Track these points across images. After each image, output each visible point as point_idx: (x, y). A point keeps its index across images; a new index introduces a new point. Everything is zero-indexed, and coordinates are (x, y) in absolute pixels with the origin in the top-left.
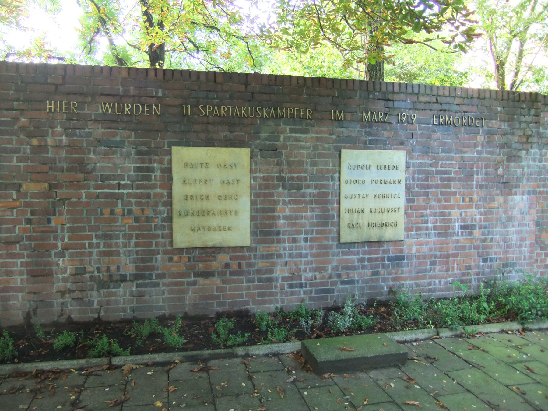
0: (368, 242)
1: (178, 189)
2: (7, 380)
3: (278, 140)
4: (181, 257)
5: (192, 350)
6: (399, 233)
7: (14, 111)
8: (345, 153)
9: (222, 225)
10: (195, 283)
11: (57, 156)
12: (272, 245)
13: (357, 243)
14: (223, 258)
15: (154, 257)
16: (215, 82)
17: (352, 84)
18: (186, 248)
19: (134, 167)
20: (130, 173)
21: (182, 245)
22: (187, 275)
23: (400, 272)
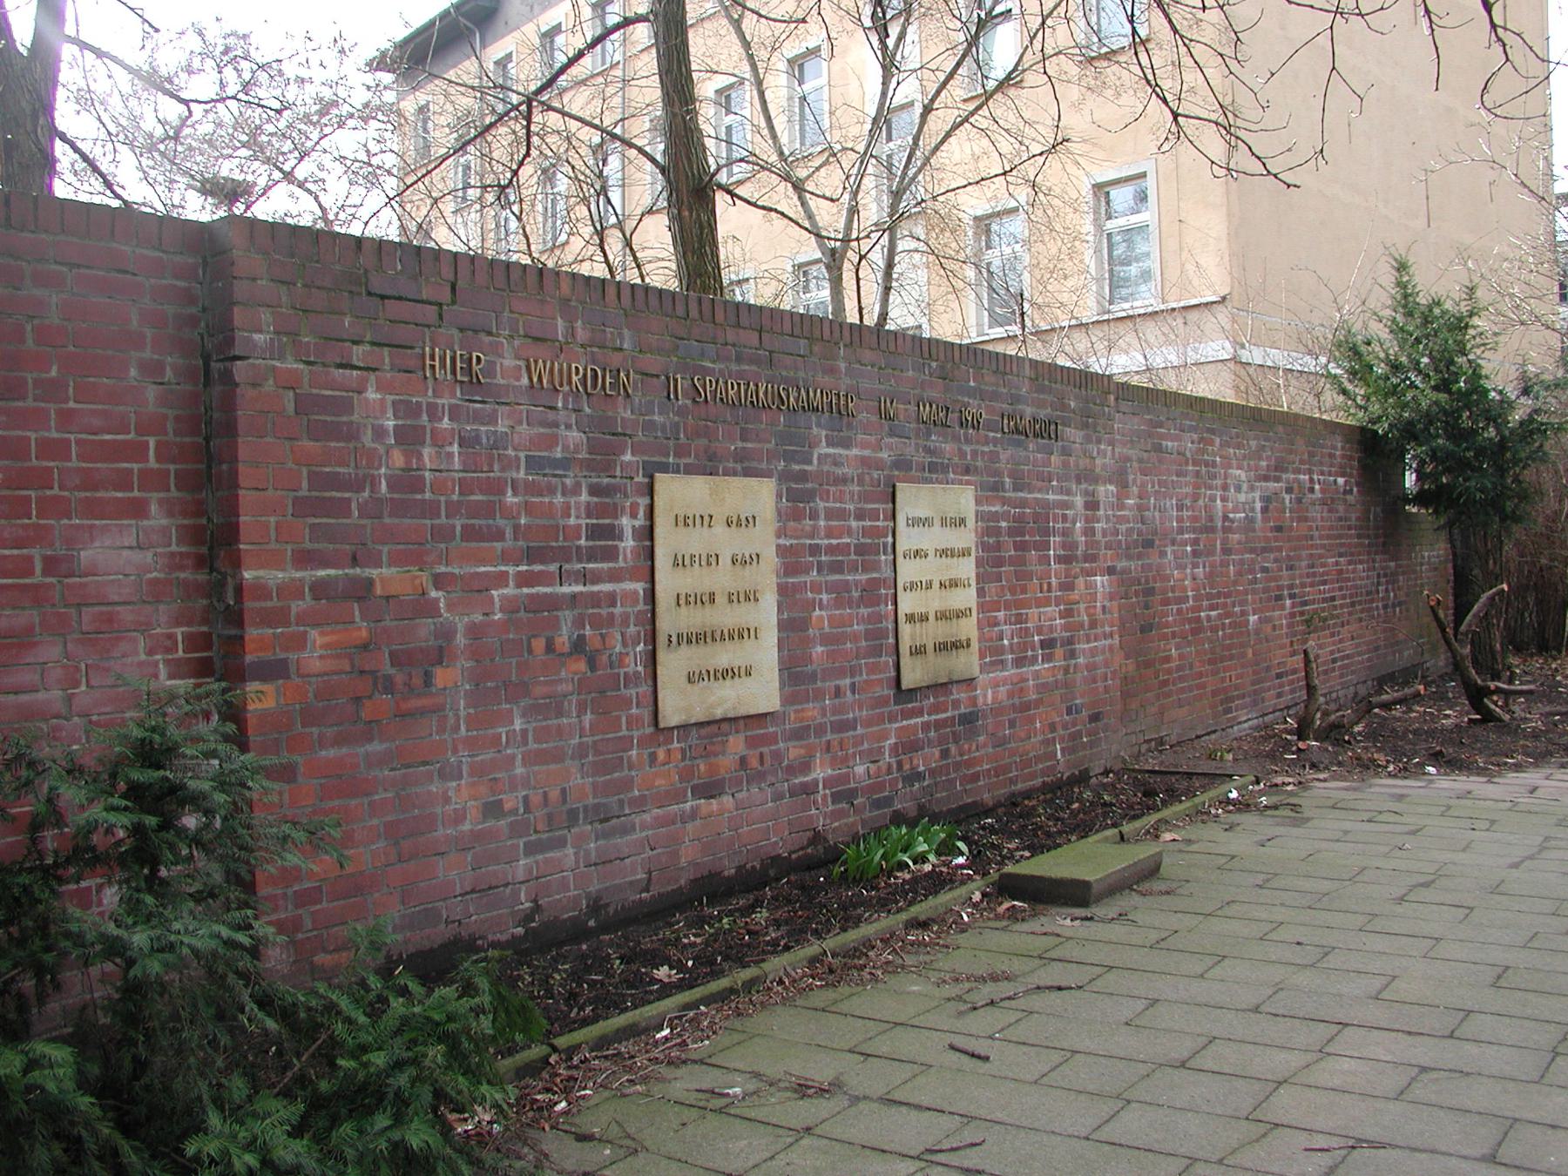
0: (936, 685)
1: (668, 582)
2: (1269, 812)
3: (810, 462)
4: (669, 750)
5: (594, 1019)
6: (968, 662)
7: (355, 372)
8: (905, 491)
9: (736, 664)
10: (694, 814)
11: (443, 499)
12: (806, 706)
13: (920, 688)
14: (736, 744)
15: (625, 755)
16: (714, 322)
17: (643, 295)
18: (677, 727)
19: (587, 525)
20: (578, 543)
21: (673, 723)
22: (679, 797)
23: (974, 747)
